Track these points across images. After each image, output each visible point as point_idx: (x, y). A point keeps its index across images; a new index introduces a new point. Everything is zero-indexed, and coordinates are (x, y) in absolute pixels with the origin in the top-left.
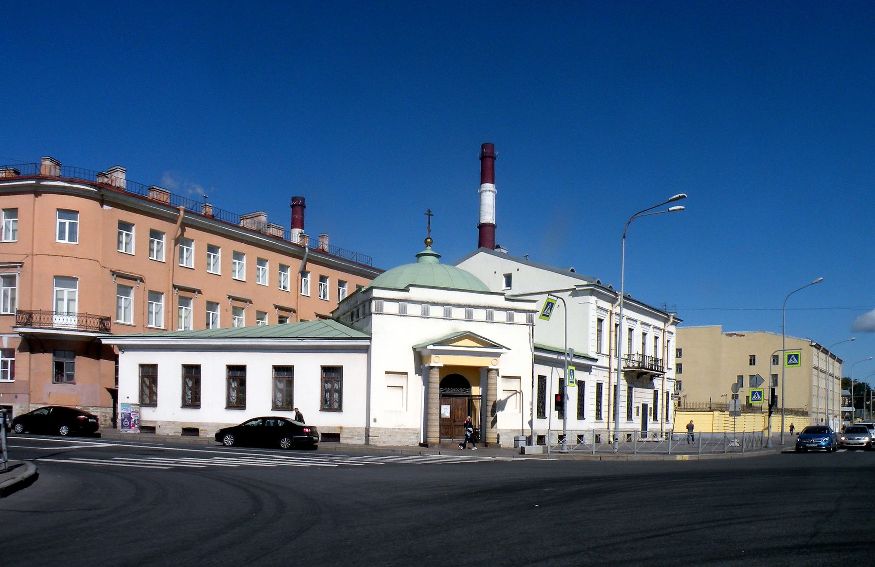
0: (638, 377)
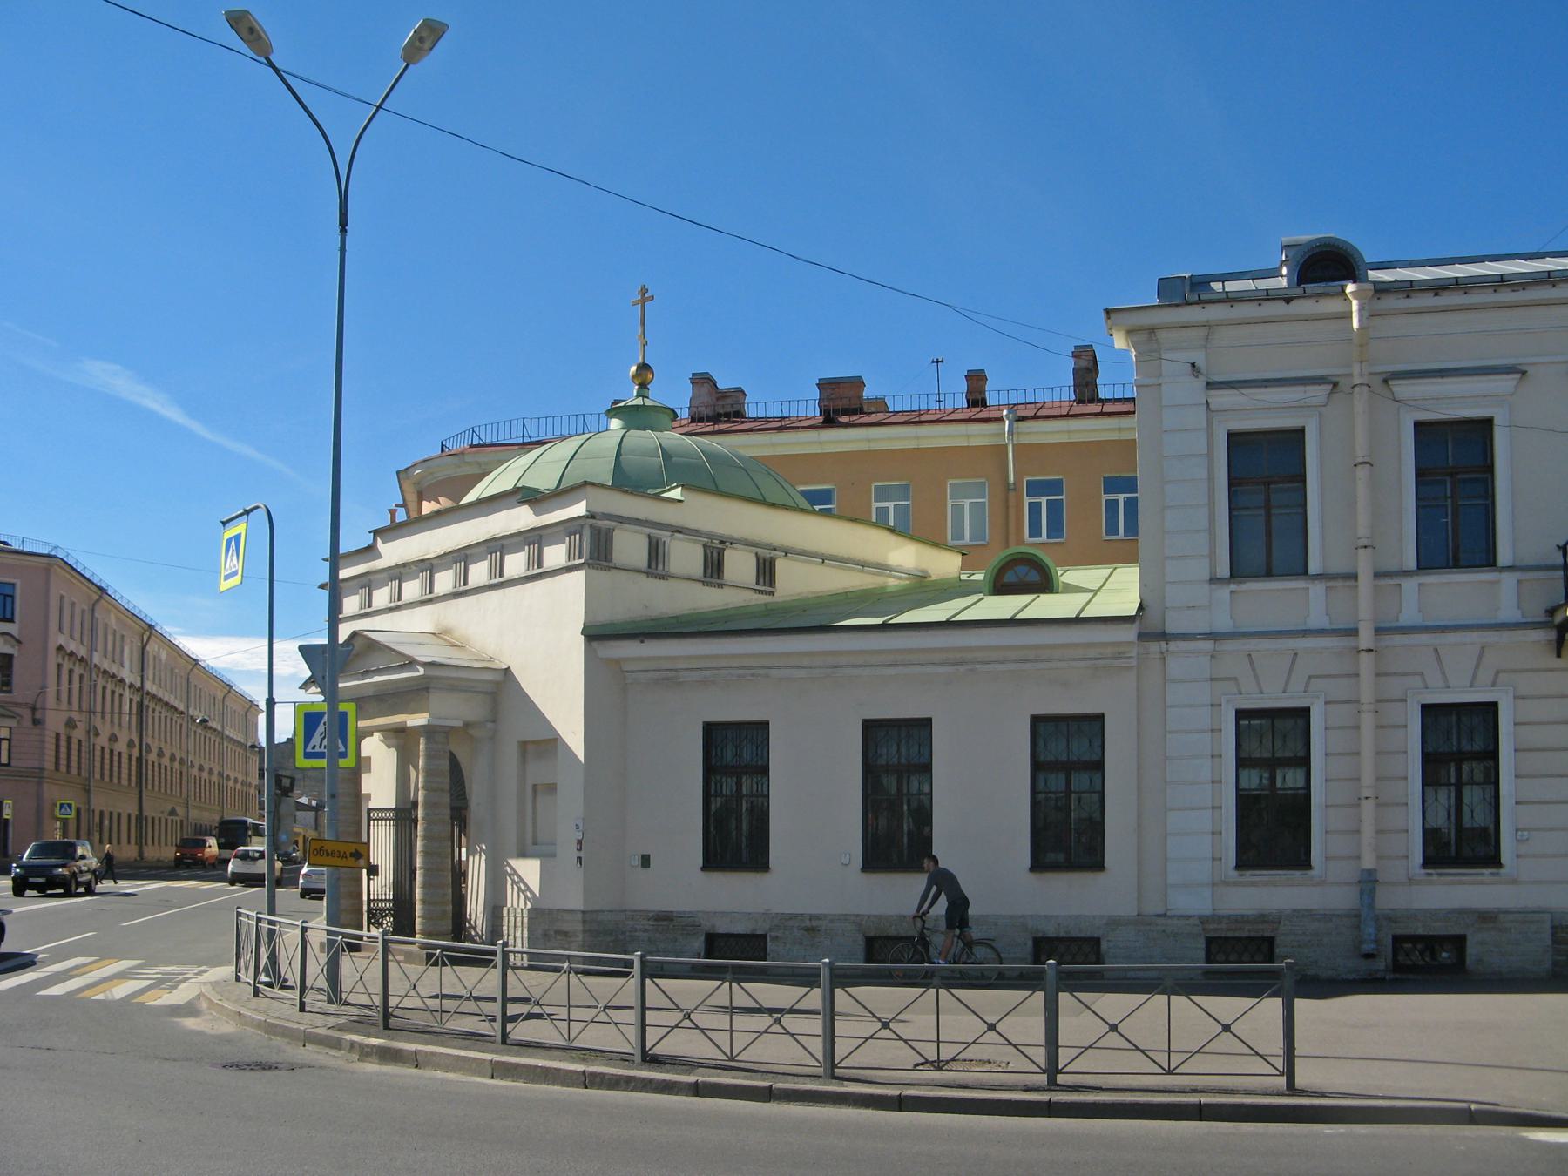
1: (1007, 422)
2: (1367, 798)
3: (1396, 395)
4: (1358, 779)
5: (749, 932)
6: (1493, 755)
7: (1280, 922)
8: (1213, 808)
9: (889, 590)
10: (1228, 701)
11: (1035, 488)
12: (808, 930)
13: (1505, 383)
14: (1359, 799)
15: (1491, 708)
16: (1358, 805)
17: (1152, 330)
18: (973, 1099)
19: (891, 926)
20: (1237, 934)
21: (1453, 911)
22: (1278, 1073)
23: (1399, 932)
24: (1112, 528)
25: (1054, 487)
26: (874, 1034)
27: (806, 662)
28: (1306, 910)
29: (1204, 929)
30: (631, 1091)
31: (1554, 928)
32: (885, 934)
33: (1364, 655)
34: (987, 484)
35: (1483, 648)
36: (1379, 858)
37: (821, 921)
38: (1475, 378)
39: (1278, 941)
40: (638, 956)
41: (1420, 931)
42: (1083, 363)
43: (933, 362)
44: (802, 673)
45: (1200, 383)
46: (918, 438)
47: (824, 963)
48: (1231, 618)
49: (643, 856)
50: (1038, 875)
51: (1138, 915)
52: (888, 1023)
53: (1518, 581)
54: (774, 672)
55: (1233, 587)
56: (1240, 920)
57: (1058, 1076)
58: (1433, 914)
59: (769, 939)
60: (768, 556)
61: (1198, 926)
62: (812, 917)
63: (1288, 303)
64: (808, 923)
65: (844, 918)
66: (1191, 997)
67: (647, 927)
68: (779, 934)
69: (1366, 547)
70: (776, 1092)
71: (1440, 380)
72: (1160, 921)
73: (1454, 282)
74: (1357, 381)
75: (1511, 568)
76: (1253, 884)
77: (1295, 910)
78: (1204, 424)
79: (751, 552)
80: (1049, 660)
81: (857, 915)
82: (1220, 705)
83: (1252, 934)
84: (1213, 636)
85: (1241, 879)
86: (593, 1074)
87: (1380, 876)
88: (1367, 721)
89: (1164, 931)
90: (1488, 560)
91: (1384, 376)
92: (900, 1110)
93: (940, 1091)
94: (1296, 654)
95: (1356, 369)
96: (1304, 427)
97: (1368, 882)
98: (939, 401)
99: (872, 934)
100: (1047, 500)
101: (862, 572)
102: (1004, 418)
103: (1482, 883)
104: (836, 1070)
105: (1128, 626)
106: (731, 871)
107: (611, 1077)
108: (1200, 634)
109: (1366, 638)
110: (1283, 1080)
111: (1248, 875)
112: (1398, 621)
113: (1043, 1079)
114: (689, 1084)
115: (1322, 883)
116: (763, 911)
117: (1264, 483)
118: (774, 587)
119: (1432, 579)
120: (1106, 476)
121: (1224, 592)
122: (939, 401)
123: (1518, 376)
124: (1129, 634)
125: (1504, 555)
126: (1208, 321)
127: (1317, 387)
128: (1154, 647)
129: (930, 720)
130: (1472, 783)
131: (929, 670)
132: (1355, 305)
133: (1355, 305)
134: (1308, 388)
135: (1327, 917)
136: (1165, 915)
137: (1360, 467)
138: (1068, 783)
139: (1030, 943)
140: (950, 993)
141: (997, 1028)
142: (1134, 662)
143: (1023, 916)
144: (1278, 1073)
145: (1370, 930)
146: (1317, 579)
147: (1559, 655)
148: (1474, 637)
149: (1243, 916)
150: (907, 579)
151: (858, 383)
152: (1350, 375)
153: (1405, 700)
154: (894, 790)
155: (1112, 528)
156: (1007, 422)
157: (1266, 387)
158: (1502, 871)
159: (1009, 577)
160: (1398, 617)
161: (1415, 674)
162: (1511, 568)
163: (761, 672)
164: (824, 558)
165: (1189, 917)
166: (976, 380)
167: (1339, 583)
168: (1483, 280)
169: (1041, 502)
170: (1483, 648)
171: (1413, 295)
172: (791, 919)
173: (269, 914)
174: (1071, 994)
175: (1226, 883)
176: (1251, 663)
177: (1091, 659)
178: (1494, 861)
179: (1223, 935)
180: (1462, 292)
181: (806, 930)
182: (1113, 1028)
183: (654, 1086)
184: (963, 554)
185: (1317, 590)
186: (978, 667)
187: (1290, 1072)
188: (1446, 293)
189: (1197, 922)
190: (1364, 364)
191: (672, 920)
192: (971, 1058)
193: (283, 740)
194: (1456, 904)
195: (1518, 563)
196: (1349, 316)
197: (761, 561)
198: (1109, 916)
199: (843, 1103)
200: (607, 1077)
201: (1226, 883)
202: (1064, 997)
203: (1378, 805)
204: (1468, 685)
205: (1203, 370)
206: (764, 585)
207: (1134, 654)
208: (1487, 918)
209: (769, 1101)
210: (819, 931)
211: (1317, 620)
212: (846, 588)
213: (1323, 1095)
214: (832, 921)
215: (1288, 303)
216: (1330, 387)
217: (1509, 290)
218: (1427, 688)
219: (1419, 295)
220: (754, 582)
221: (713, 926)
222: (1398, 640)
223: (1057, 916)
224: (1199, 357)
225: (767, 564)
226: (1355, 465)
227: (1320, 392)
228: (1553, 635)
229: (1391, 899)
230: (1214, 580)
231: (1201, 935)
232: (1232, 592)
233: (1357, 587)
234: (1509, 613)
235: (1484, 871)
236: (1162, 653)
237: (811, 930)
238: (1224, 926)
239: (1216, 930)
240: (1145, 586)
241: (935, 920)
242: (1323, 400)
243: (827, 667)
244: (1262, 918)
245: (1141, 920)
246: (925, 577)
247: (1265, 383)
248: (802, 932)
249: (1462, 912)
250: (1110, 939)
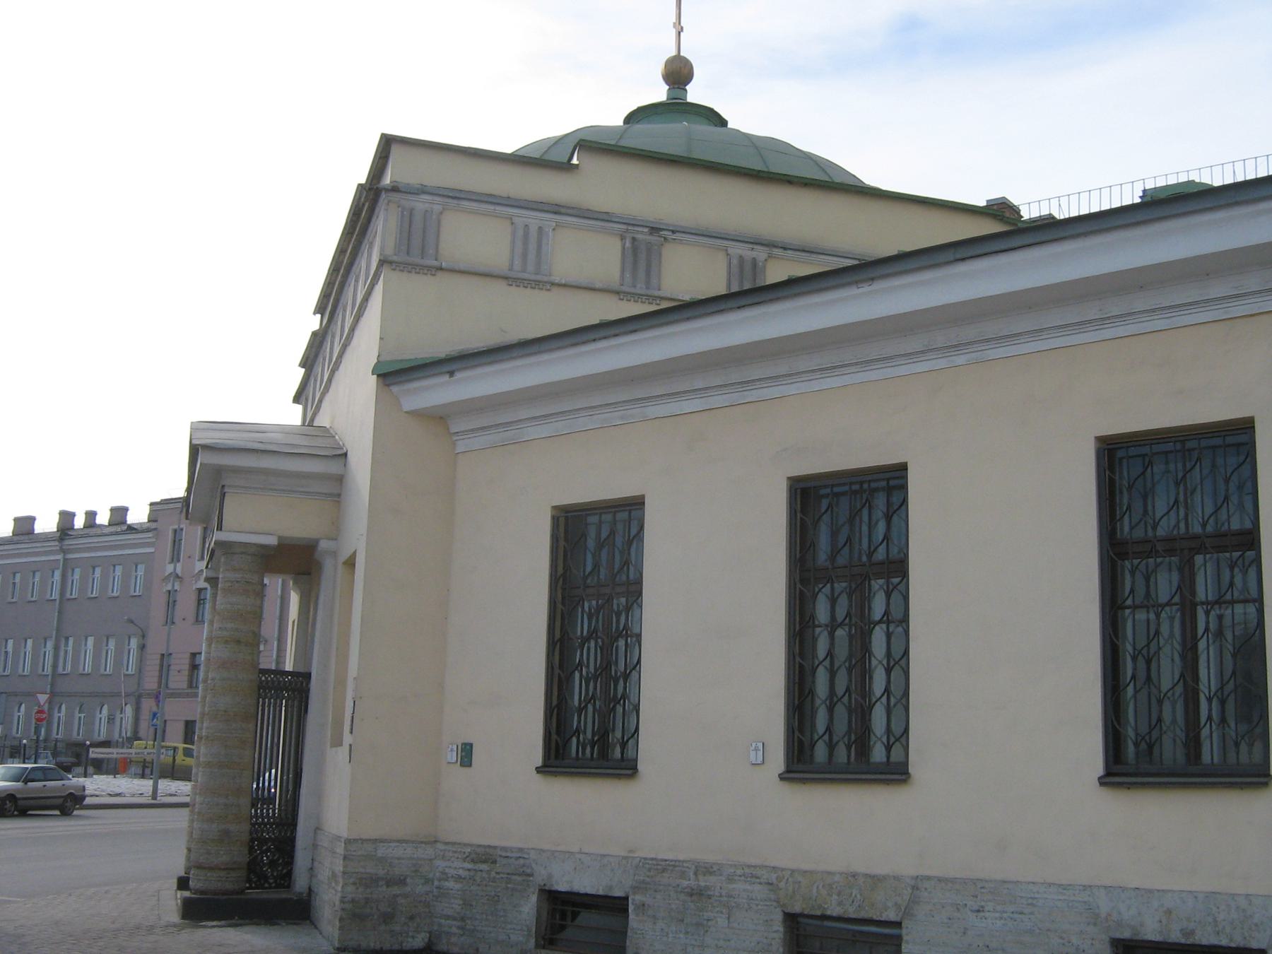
5: (601, 893)
49: (465, 745)
65: (751, 874)
67: (461, 872)
154: (176, 584)
172: (664, 870)
173: (215, 541)
191: (495, 862)
193: (1256, 743)
210: (709, 897)
221: (550, 876)
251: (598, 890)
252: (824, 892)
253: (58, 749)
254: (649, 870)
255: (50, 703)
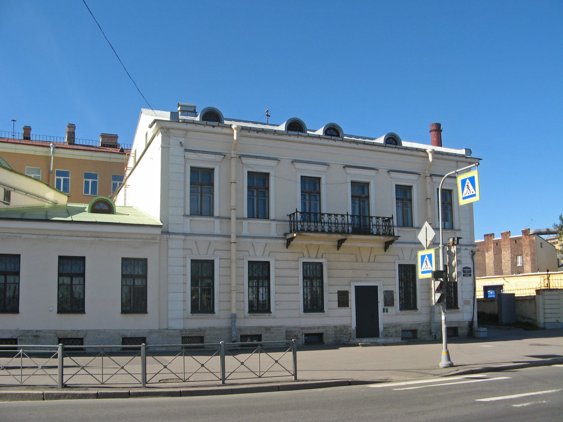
0: (386, 249)
1: (52, 148)
2: (234, 290)
3: (242, 162)
4: (230, 284)
6: (268, 278)
7: (206, 331)
8: (183, 292)
9: (46, 207)
10: (189, 256)
11: (59, 173)
12: (35, 336)
13: (323, 168)
14: (231, 291)
15: (268, 263)
16: (231, 293)
17: (168, 129)
18: (197, 391)
19: (69, 334)
20: (192, 335)
21: (258, 327)
22: (219, 379)
23: (242, 334)
24: (87, 191)
25: (65, 174)
26: (116, 373)
27: (37, 232)
28: (213, 327)
29: (181, 334)
30: (67, 399)
31: (286, 332)
32: (66, 337)
33: (233, 244)
34: (41, 170)
35: (266, 244)
36: (237, 310)
37: (41, 333)
38: (268, 160)
39: (205, 337)
40: (60, 345)
41: (248, 334)
42: (71, 130)
43: (12, 120)
44: (35, 237)
45: (183, 149)
46: (16, 149)
47: (143, 345)
48: (190, 228)
50: (124, 315)
51: (159, 329)
52: (204, 365)
53: (276, 224)
54: (23, 236)
55: (191, 218)
56: (193, 330)
57: (225, 381)
58: (252, 328)
59: (18, 340)
60: (9, 190)
61: (179, 333)
62: (37, 331)
63: (213, 127)
64: (35, 334)
65: (50, 332)
66: (192, 356)
68: (23, 338)
69: (234, 209)
70: (131, 394)
71: (256, 159)
72: (167, 331)
73: (250, 128)
74: (233, 156)
75: (274, 220)
76: (197, 318)
77: (210, 327)
78: (183, 163)
79: (2, 187)
80: (129, 238)
81: (55, 330)
82: (186, 258)
83: (197, 335)
84: (185, 234)
85: (193, 317)
86: (47, 394)
87: (237, 316)
88: (234, 266)
89: (168, 335)
90: (211, 214)
91: (239, 155)
92: (181, 396)
93: (188, 389)
94: (210, 242)
95: (233, 152)
96: (214, 168)
97: (234, 318)
98: (14, 136)
99: (61, 337)
100: (64, 178)
101: (37, 199)
102: (51, 147)
103: (265, 318)
104: (146, 385)
105: (159, 229)
106: (62, 314)
107: (57, 394)
108: (180, 233)
109: (233, 239)
110: (293, 377)
111: (403, 312)
112: (241, 234)
113: (221, 382)
114: (94, 394)
115: (218, 318)
116: (16, 329)
117: (201, 185)
118: (10, 202)
119: (252, 221)
120: (113, 174)
121: (188, 220)
122: (14, 136)
123: (278, 161)
124: (158, 231)
125: (272, 215)
126: (187, 129)
127: (219, 156)
128: (165, 236)
129: (84, 257)
130: (263, 286)
131: (86, 239)
132: (235, 132)
133: (235, 132)
134: (217, 156)
135: (220, 329)
136: (167, 329)
137: (232, 183)
138: (72, 281)
139: (121, 340)
140: (154, 358)
141: (278, 362)
142: (158, 241)
143: (119, 330)
144: (219, 379)
145: (234, 333)
146: (217, 218)
147: (287, 248)
148: (264, 241)
149: (194, 329)
150: (51, 204)
151: (116, 137)
152: (231, 154)
153: (244, 259)
155: (87, 191)
156: (52, 148)
157: (204, 153)
158: (271, 314)
159: (97, 207)
160: (241, 232)
161: (246, 251)
162: (274, 220)
163: (18, 235)
164: (27, 193)
165: (176, 330)
166: (27, 129)
167: (224, 220)
168: (271, 131)
169: (89, 181)
170: (266, 244)
171: (251, 131)
174: (109, 357)
175: (188, 318)
176: (196, 244)
177: (144, 239)
178: (268, 311)
179: (187, 336)
180: (264, 133)
181: (34, 336)
182: (203, 365)
183: (77, 396)
184: (68, 196)
185: (217, 222)
186: (104, 239)
187: (295, 375)
188: (260, 133)
189: (179, 331)
190: (235, 151)
192: (173, 378)
194: (258, 325)
195: (276, 219)
196: (233, 135)
197: (6, 191)
198: (149, 330)
199: (159, 396)
200: (55, 395)
201: (188, 318)
202: (149, 359)
203: (237, 293)
204: (262, 255)
205: (184, 145)
206: (7, 201)
207: (158, 238)
208: (268, 329)
209: (129, 398)
210: (40, 336)
211: (217, 231)
212: (32, 205)
213: (307, 381)
214: (45, 333)
215: (213, 127)
216: (223, 156)
217: (278, 135)
218: (250, 256)
219: (252, 132)
220: (3, 200)
222: (242, 240)
223: (131, 330)
224: (183, 140)
225: (8, 193)
226: (231, 183)
227: (220, 157)
228: (286, 242)
229: (240, 323)
230: (185, 215)
231: (180, 336)
232: (190, 220)
233: (231, 222)
234: (273, 234)
235: (266, 314)
236: (167, 239)
237: (36, 336)
238: (188, 333)
239: (186, 334)
240: (162, 215)
241: (86, 332)
242: (221, 160)
243: (45, 235)
244: (200, 330)
245: (160, 331)
246: (56, 203)
247: (203, 152)
248: (33, 337)
249: (260, 327)
250: (149, 338)
251: (85, 341)
252: (68, 334)
253: (489, 296)
254: (24, 332)
255: (366, 197)
